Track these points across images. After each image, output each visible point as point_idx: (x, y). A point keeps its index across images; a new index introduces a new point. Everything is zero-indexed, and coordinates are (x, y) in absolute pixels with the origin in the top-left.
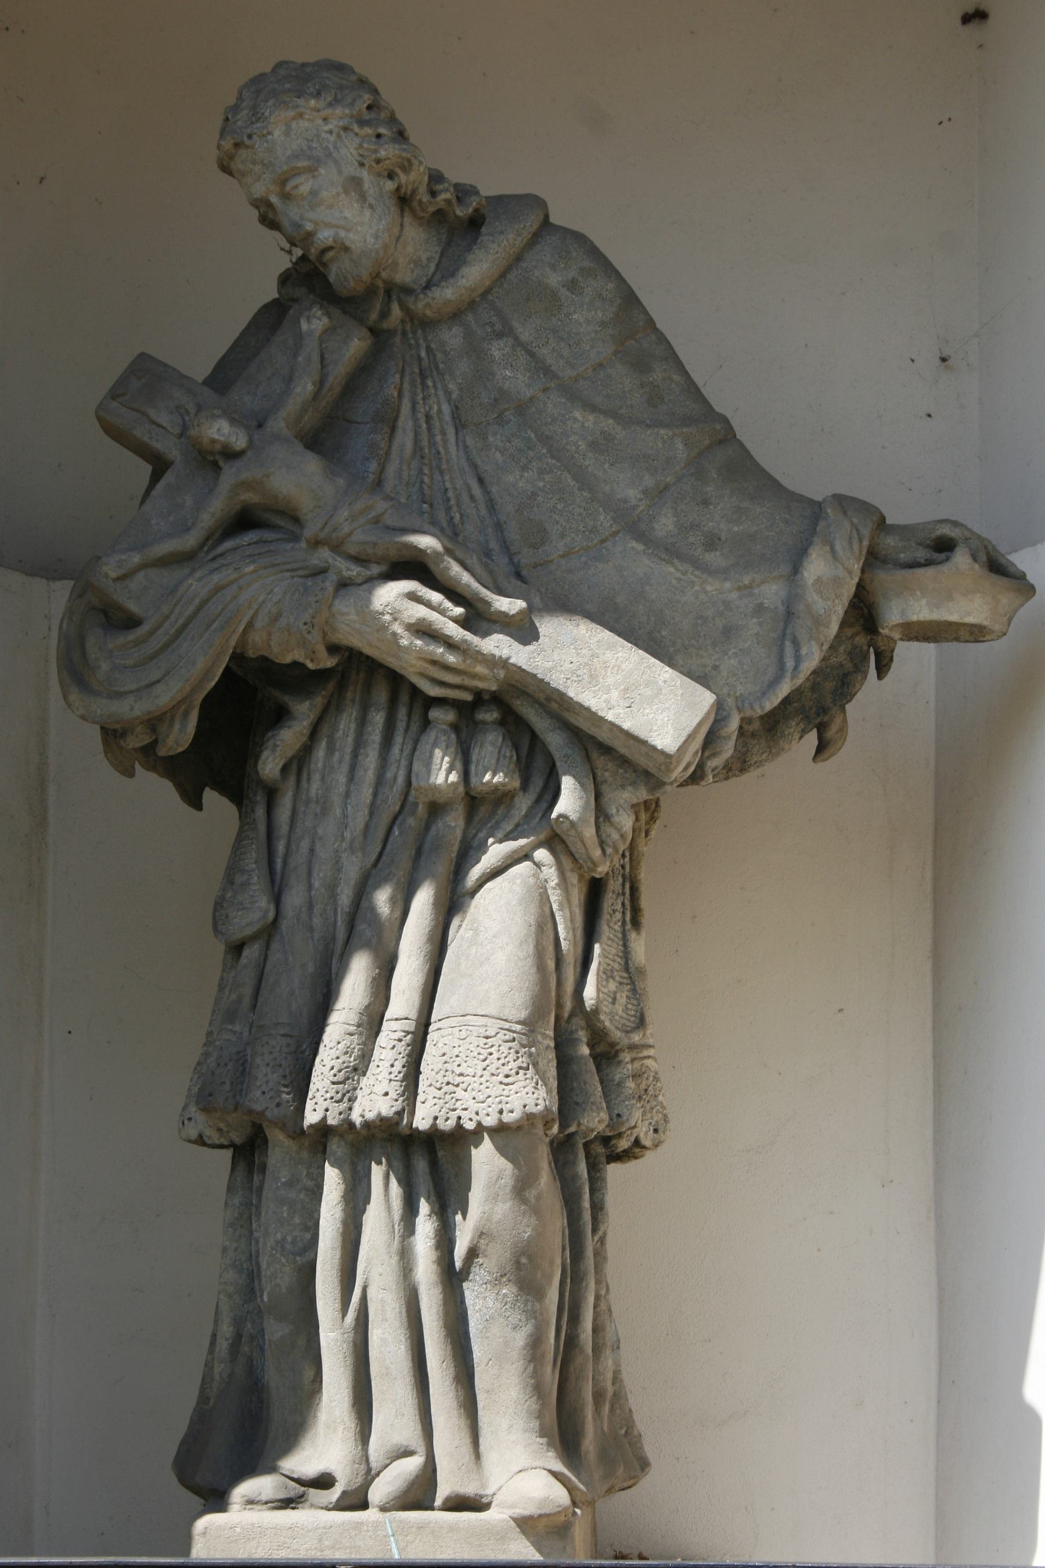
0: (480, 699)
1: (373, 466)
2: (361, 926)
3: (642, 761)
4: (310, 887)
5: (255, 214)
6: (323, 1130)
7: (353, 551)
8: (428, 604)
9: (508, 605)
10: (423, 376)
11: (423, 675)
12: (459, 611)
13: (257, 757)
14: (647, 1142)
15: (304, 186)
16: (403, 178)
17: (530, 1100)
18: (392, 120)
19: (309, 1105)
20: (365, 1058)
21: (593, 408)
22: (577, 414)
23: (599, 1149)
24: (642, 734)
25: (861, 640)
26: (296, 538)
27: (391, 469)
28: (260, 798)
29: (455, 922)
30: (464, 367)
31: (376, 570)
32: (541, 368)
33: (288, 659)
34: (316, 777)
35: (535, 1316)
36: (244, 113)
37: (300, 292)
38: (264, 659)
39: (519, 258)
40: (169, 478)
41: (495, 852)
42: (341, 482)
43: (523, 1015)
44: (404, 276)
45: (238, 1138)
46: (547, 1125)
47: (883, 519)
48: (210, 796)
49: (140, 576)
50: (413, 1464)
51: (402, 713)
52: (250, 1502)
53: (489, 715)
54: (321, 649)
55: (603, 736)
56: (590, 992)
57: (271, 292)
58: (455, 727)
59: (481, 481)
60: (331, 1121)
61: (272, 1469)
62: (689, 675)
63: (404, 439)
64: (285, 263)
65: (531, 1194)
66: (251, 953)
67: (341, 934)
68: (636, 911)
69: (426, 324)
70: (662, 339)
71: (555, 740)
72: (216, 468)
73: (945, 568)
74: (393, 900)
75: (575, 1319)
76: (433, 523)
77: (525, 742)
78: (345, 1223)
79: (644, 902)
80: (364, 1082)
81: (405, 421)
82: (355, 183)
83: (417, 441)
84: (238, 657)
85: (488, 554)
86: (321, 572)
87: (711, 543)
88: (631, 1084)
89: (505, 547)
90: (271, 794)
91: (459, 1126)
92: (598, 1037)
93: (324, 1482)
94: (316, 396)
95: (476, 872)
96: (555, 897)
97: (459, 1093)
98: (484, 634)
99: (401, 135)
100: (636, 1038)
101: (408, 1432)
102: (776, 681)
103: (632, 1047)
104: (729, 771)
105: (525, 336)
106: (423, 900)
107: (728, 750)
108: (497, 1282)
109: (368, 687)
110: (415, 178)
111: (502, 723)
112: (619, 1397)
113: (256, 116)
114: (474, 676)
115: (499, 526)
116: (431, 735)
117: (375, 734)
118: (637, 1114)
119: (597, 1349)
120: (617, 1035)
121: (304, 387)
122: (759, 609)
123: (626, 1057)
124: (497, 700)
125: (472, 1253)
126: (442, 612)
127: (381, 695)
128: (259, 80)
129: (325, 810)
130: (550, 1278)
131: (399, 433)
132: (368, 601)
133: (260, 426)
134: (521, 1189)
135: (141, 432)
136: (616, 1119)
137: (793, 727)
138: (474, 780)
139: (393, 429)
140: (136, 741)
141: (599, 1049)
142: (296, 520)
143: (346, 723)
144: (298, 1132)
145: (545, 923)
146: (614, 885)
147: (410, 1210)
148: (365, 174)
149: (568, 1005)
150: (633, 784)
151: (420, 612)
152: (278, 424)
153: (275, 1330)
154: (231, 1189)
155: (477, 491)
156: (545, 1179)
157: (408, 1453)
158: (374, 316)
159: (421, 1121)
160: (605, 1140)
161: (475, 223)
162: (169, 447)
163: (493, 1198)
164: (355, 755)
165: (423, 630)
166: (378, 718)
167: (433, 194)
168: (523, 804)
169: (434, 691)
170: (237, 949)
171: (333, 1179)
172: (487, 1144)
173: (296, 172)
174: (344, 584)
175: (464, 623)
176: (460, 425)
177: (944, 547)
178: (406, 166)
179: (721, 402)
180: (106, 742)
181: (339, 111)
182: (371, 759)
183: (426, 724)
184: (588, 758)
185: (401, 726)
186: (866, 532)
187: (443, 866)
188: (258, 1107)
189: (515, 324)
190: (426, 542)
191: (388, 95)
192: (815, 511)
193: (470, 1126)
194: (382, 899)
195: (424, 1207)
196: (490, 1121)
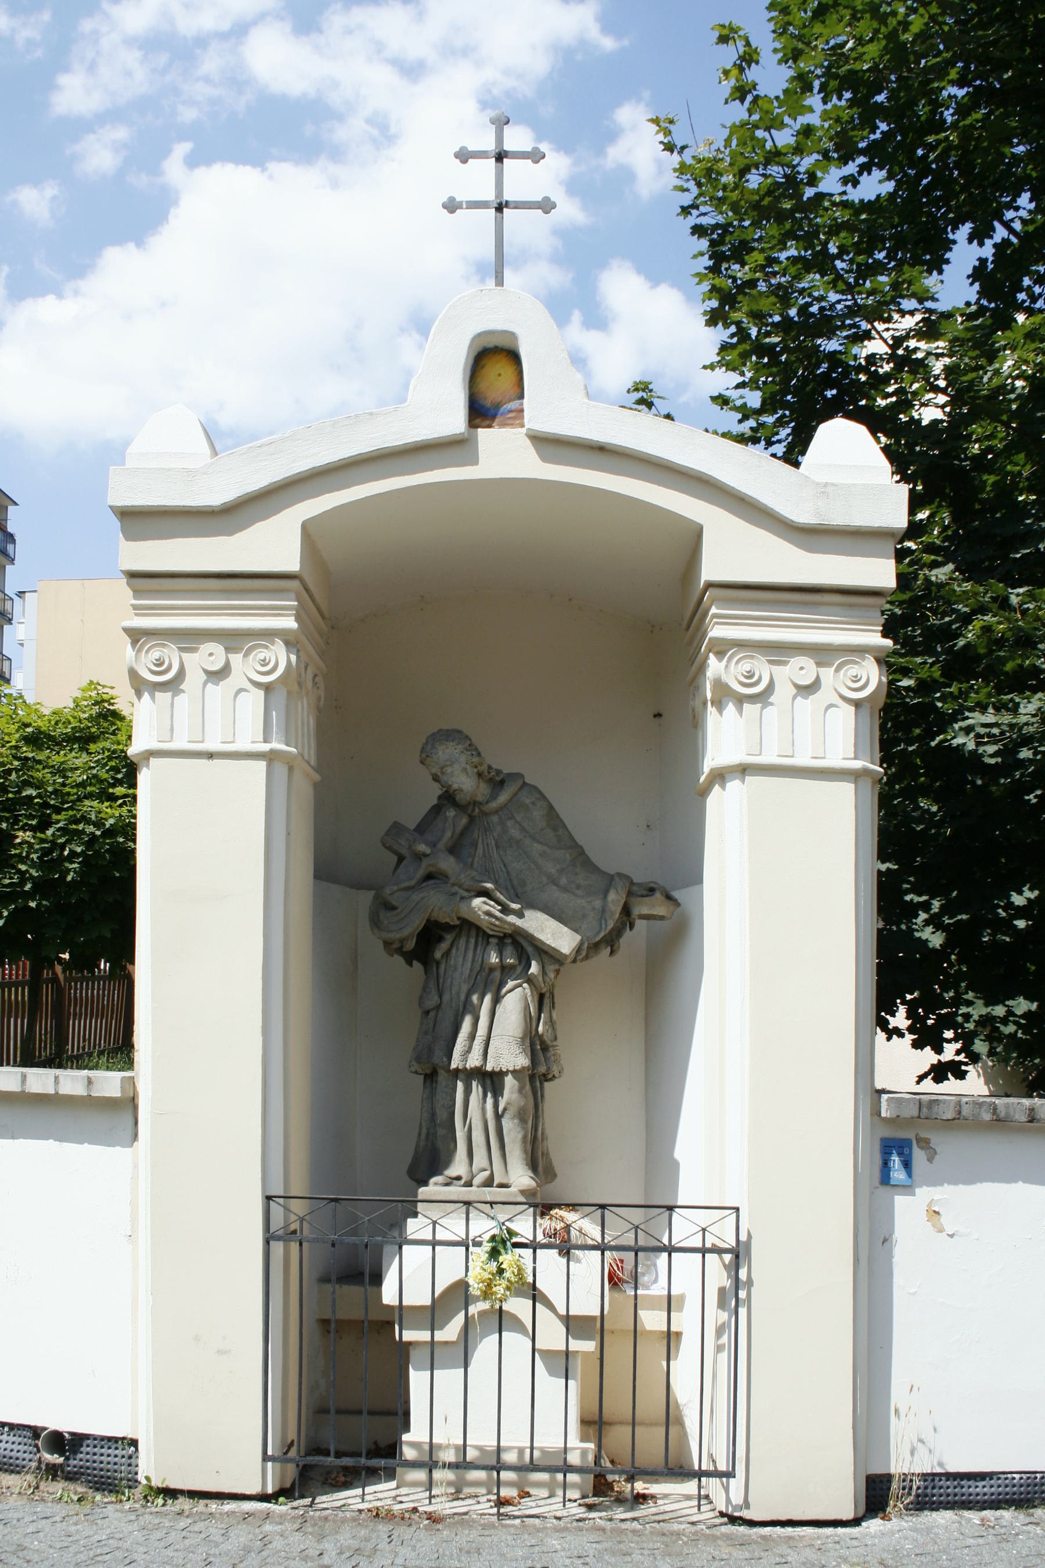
0: (506, 936)
1: (470, 860)
2: (468, 1006)
3: (558, 957)
4: (451, 993)
5: (431, 777)
6: (457, 1070)
7: (465, 887)
8: (490, 905)
9: (515, 906)
10: (486, 831)
11: (488, 928)
12: (500, 908)
13: (434, 952)
14: (556, 1076)
15: (449, 770)
16: (480, 768)
17: (524, 1062)
18: (476, 749)
19: (452, 1062)
20: (470, 1048)
21: (540, 843)
22: (535, 845)
23: (542, 1078)
24: (558, 948)
25: (625, 919)
26: (446, 883)
27: (476, 860)
28: (434, 965)
29: (498, 1006)
30: (499, 829)
31: (473, 894)
32: (523, 829)
33: (444, 921)
34: (453, 959)
35: (524, 1129)
36: (429, 746)
37: (445, 802)
38: (436, 921)
39: (516, 794)
40: (405, 862)
41: (511, 984)
42: (461, 865)
43: (520, 1036)
44: (480, 798)
45: (428, 1072)
46: (528, 1070)
47: (632, 881)
48: (415, 963)
49: (397, 894)
50: (487, 1173)
51: (480, 939)
52: (436, 1184)
53: (508, 941)
54: (455, 919)
55: (545, 948)
56: (540, 1029)
57: (435, 802)
58: (498, 944)
59: (505, 865)
60: (460, 1067)
61: (441, 1174)
62: (572, 929)
63: (480, 851)
64: (440, 792)
65: (524, 1092)
66: (432, 1014)
67: (461, 1009)
68: (553, 1003)
69: (486, 814)
70: (561, 821)
71: (530, 949)
72: (420, 859)
73: (652, 897)
74: (478, 999)
75: (536, 1130)
76: (490, 878)
77: (520, 950)
78: (464, 1099)
79: (556, 1001)
80: (470, 1055)
81: (480, 845)
82: (465, 769)
83: (484, 852)
84: (428, 920)
85: (507, 889)
86: (455, 894)
87: (578, 887)
88: (552, 1058)
89: (513, 887)
90: (438, 963)
91: (501, 1070)
92: (543, 1043)
93: (459, 1178)
94: (452, 837)
95: (504, 990)
96: (529, 999)
97: (501, 1060)
98: (507, 915)
99: (479, 754)
100: (554, 1043)
101: (485, 1163)
102: (598, 933)
103: (553, 1046)
104: (582, 960)
105: (518, 819)
106: (488, 999)
107: (584, 953)
108: (513, 1118)
109: (469, 930)
110: (484, 768)
111: (512, 943)
112: (548, 1154)
113: (433, 747)
114: (504, 928)
115: (511, 880)
116: (490, 947)
117: (472, 946)
118: (555, 1068)
119: (542, 1140)
120: (549, 1042)
121: (448, 834)
122: (594, 909)
123: (551, 1049)
124: (511, 936)
125: (505, 1109)
126: (494, 908)
127: (473, 933)
128: (433, 734)
129: (456, 969)
130: (529, 1117)
131: (478, 850)
132: (470, 904)
133: (435, 846)
134: (521, 1090)
135: (396, 847)
136: (549, 1069)
137: (603, 945)
138: (504, 962)
139: (476, 848)
140: (396, 946)
141: (543, 1046)
142: (447, 877)
143: (462, 942)
144: (448, 1071)
145: (527, 1007)
146: (547, 995)
147: (485, 1096)
148: (468, 766)
149: (534, 1033)
150: (554, 964)
151: (487, 908)
152: (441, 845)
153: (441, 1132)
154: (425, 1087)
155: (504, 869)
156: (528, 1087)
157: (485, 1170)
158: (470, 811)
159: (489, 1068)
160: (544, 1075)
161: (502, 782)
162: (404, 852)
163: (512, 1092)
164: (465, 951)
165: (488, 913)
166: (473, 941)
167: (489, 773)
168: (519, 969)
169: (491, 933)
170: (427, 1013)
171: (460, 1086)
172: (510, 1076)
173: (447, 766)
174: (462, 898)
175: (501, 911)
176: (497, 847)
177: (652, 891)
178: (481, 764)
179: (580, 840)
180: (385, 946)
181: (460, 746)
182: (470, 954)
183: (488, 943)
184: (540, 955)
185: (480, 943)
186: (627, 885)
187: (494, 988)
188: (436, 1062)
189: (515, 815)
190: (489, 885)
191: (474, 740)
192: (611, 878)
193: (504, 1070)
194: (475, 998)
195: (489, 1095)
196: (511, 1069)
